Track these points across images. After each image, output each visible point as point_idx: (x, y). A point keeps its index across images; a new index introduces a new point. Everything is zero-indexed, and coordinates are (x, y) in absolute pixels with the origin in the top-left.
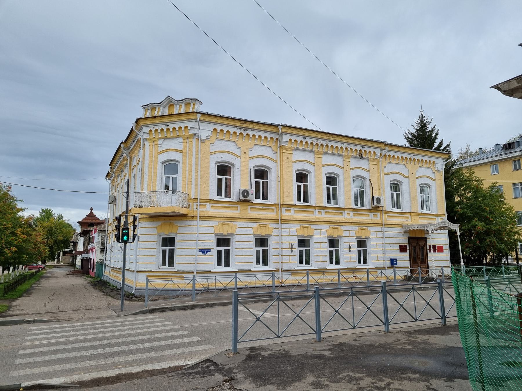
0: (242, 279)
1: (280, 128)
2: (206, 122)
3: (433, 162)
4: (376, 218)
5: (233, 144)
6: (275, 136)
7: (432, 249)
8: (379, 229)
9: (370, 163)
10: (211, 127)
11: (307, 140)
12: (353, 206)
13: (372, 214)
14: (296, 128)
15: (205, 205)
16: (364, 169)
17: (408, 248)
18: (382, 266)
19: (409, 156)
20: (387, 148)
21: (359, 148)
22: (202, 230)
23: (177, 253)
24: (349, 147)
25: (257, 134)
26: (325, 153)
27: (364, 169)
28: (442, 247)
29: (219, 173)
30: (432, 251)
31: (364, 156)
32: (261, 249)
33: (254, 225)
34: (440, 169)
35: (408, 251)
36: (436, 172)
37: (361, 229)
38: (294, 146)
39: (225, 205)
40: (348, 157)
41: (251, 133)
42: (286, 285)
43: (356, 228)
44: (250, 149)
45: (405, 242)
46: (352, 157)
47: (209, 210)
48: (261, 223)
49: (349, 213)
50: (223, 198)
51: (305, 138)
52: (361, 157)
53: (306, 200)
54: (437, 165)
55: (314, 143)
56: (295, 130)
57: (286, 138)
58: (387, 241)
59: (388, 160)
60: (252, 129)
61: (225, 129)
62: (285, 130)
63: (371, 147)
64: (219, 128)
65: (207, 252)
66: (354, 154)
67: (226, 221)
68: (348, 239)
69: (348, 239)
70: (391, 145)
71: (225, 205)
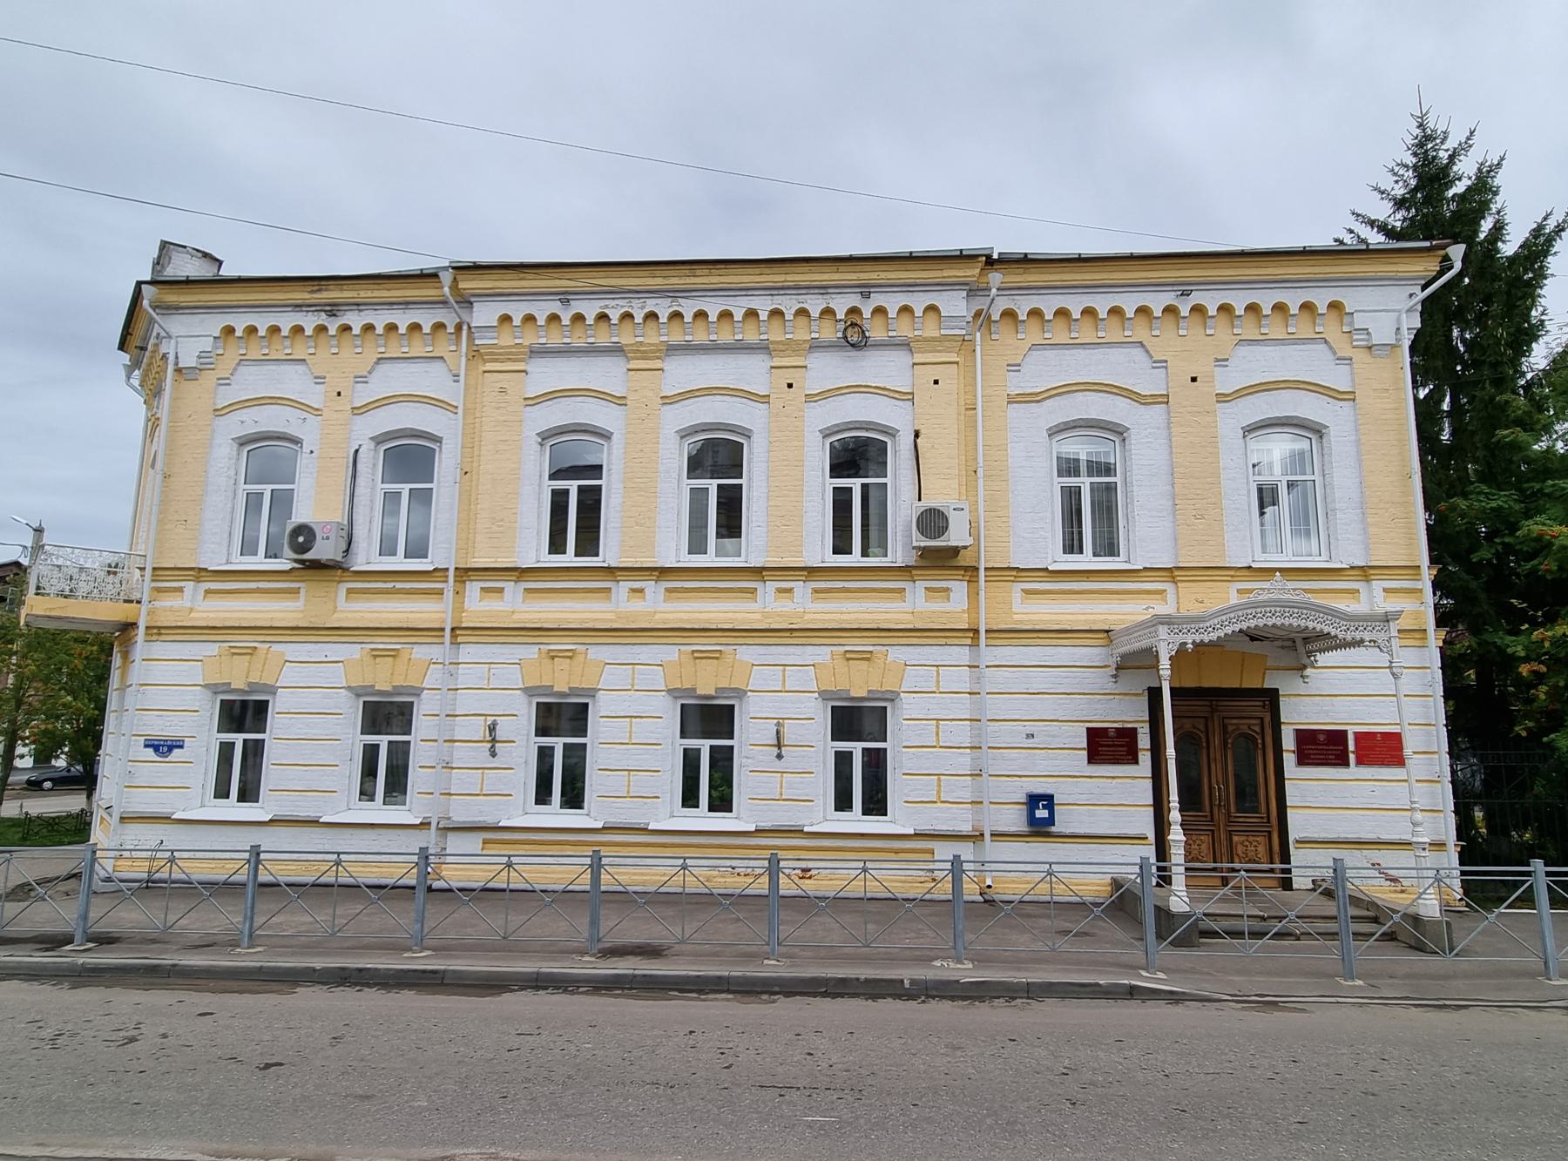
1: (446, 278)
2: (176, 309)
3: (1335, 306)
4: (938, 606)
5: (1138, 353)
6: (449, 318)
8: (961, 654)
9: (918, 358)
10: (214, 324)
11: (1197, 298)
13: (921, 585)
14: (911, 258)
15: (180, 590)
16: (882, 391)
17: (1144, 741)
18: (966, 828)
19: (1157, 302)
20: (995, 278)
21: (841, 304)
22: (159, 672)
23: (273, 752)
24: (789, 305)
25: (380, 320)
26: (672, 350)
27: (882, 391)
29: (837, 469)
31: (876, 332)
32: (705, 745)
33: (353, 651)
34: (1382, 331)
36: (1360, 356)
37: (849, 657)
38: (530, 338)
39: (253, 585)
40: (790, 347)
41: (356, 320)
42: (455, 885)
43: (821, 654)
44: (361, 379)
46: (816, 346)
47: (194, 604)
48: (382, 642)
49: (641, 591)
50: (1086, 560)
52: (854, 338)
53: (1108, 546)
54: (1360, 321)
55: (615, 316)
56: (511, 274)
57: (484, 314)
58: (997, 707)
59: (1032, 334)
60: (358, 306)
61: (262, 322)
62: (468, 284)
63: (909, 287)
64: (240, 322)
65: (171, 749)
66: (830, 332)
67: (246, 641)
68: (784, 704)
69: (784, 704)
70: (1025, 261)
71: (253, 585)
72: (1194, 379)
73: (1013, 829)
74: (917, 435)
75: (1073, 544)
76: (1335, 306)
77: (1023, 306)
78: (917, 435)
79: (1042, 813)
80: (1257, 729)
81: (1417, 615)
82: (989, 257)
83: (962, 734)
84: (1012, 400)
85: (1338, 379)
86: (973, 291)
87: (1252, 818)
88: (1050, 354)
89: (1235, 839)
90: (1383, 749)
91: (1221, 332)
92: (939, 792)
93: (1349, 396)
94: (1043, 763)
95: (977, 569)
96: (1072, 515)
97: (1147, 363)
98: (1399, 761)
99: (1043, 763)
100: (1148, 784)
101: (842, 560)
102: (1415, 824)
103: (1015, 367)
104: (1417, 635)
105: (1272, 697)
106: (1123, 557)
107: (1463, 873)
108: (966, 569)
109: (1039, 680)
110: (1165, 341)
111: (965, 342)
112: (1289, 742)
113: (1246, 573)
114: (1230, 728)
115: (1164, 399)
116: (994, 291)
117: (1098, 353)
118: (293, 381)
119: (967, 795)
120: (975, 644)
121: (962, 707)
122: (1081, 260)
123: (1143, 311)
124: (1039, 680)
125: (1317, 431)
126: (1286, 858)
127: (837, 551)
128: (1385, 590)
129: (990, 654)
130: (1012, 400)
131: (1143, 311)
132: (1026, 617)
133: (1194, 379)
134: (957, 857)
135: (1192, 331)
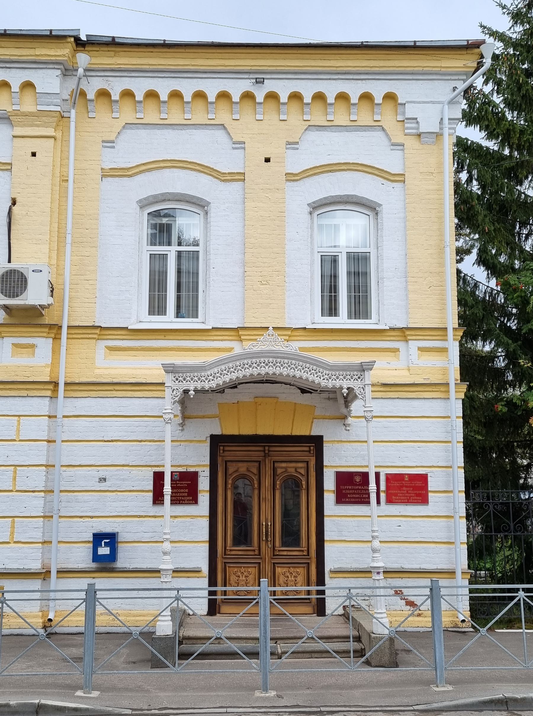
0: (111, 604)
3: (390, 97)
5: (220, 134)
7: (167, 489)
8: (42, 405)
9: (18, 131)
11: (270, 86)
12: (140, 317)
17: (204, 484)
18: (36, 566)
19: (237, 88)
20: (83, 59)
28: (424, 478)
30: (167, 499)
35: (204, 498)
36: (411, 143)
45: (198, 460)
50: (169, 320)
51: (259, 82)
54: (410, 111)
58: (70, 454)
59: (127, 114)
72: (267, 160)
73: (82, 566)
74: (14, 203)
75: (157, 307)
76: (390, 97)
77: (116, 86)
78: (14, 203)
79: (104, 551)
80: (303, 471)
81: (445, 371)
82: (77, 40)
83: (37, 479)
84: (107, 174)
85: (392, 162)
86: (68, 71)
87: (294, 551)
88: (143, 133)
89: (279, 570)
90: (410, 489)
91: (294, 118)
92: (12, 533)
93: (398, 178)
94: (114, 504)
95: (60, 327)
96: (157, 283)
97: (228, 144)
98: (424, 500)
99: (114, 504)
100: (205, 523)
101: (331, 322)
102: (374, 551)
103: (109, 144)
104: (443, 389)
105: (317, 442)
106: (201, 318)
107: (471, 591)
108: (51, 326)
109: (115, 429)
110: (247, 124)
111: (62, 117)
112: (330, 483)
113: (301, 333)
114: (279, 471)
115: (239, 177)
116: (81, 71)
117: (185, 134)
118: (206, 146)
119: (38, 536)
120: (54, 397)
121: (38, 454)
122: (165, 46)
123: (224, 96)
124: (115, 429)
125: (371, 207)
126: (321, 581)
127: (151, 312)
128: (419, 349)
129: (66, 405)
130: (107, 174)
131: (366, 97)
132: (106, 372)
133: (267, 160)
134: (91, 585)
135: (270, 117)
